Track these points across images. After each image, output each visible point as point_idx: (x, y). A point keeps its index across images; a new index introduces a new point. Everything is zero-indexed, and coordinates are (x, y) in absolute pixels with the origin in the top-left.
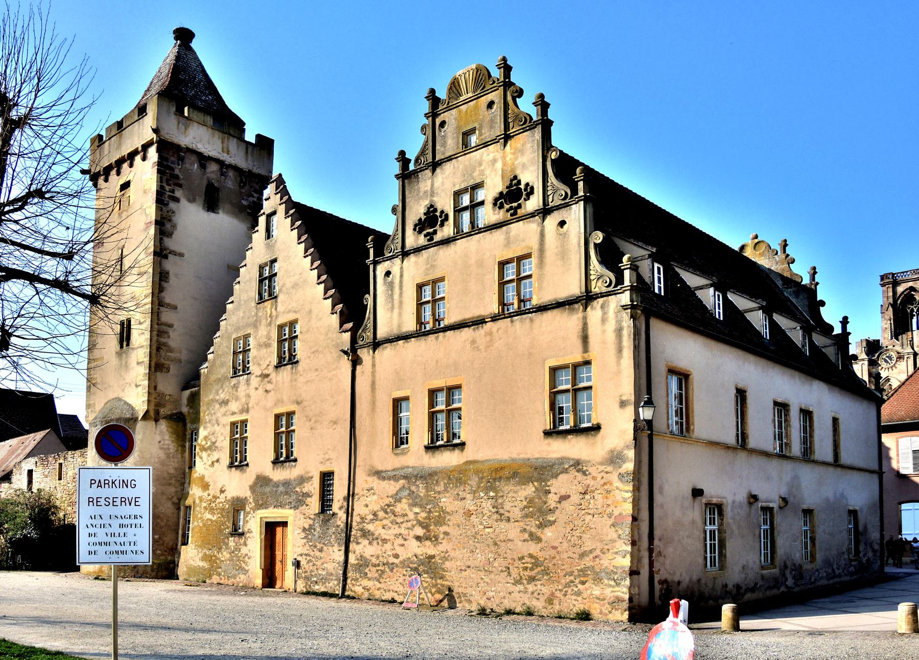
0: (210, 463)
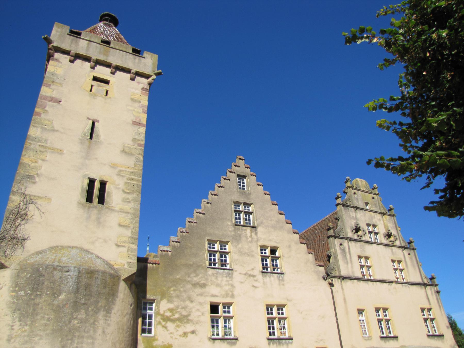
0: (181, 331)
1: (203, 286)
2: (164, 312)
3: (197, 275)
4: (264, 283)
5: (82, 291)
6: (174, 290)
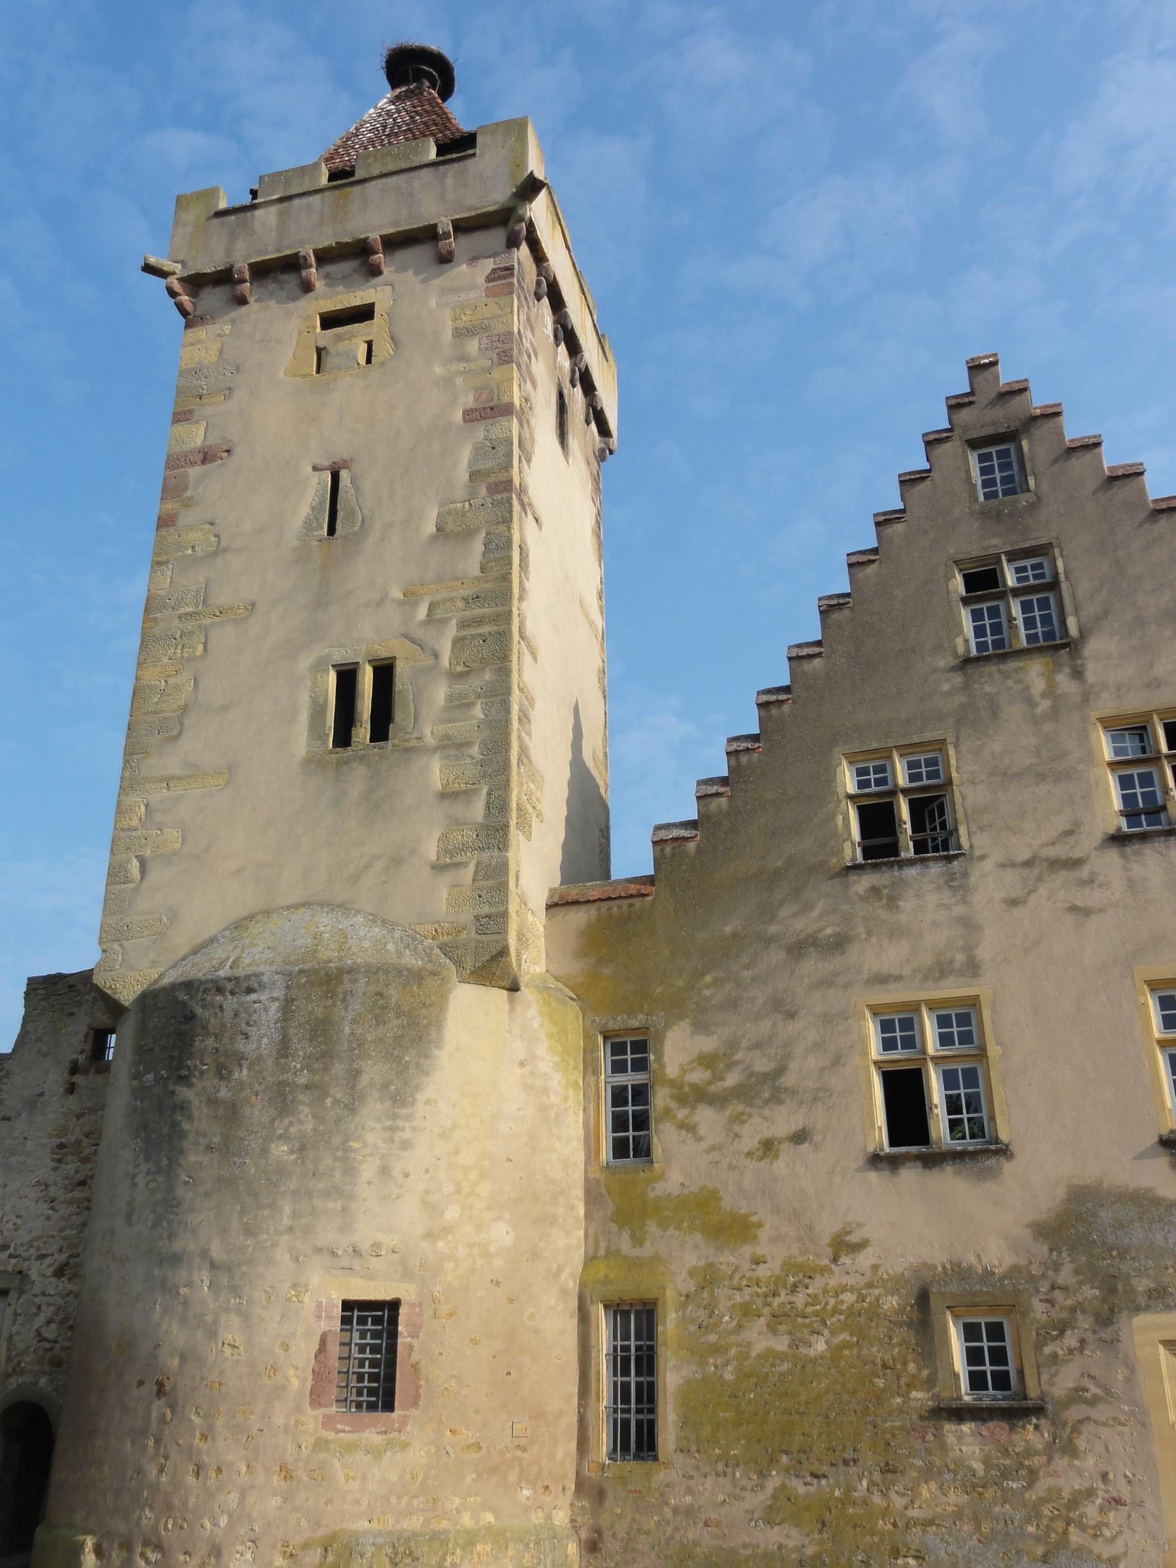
0: (750, 1138)
1: (840, 943)
2: (683, 1071)
3: (809, 907)
4: (1132, 884)
5: (301, 1047)
6: (716, 983)
